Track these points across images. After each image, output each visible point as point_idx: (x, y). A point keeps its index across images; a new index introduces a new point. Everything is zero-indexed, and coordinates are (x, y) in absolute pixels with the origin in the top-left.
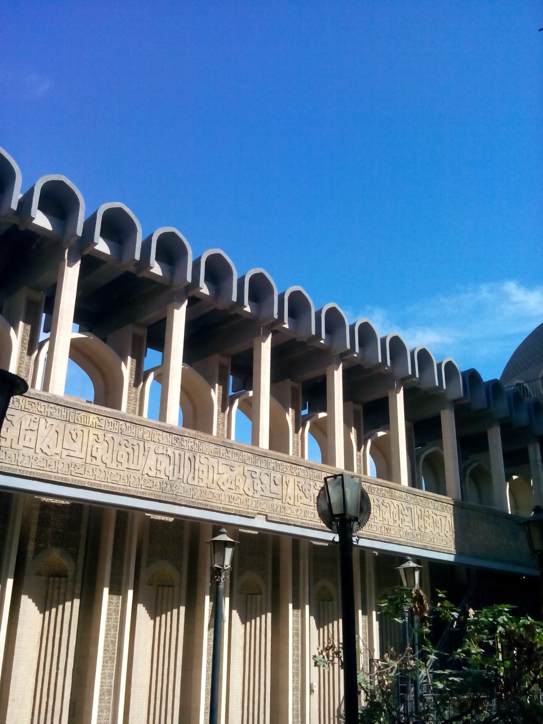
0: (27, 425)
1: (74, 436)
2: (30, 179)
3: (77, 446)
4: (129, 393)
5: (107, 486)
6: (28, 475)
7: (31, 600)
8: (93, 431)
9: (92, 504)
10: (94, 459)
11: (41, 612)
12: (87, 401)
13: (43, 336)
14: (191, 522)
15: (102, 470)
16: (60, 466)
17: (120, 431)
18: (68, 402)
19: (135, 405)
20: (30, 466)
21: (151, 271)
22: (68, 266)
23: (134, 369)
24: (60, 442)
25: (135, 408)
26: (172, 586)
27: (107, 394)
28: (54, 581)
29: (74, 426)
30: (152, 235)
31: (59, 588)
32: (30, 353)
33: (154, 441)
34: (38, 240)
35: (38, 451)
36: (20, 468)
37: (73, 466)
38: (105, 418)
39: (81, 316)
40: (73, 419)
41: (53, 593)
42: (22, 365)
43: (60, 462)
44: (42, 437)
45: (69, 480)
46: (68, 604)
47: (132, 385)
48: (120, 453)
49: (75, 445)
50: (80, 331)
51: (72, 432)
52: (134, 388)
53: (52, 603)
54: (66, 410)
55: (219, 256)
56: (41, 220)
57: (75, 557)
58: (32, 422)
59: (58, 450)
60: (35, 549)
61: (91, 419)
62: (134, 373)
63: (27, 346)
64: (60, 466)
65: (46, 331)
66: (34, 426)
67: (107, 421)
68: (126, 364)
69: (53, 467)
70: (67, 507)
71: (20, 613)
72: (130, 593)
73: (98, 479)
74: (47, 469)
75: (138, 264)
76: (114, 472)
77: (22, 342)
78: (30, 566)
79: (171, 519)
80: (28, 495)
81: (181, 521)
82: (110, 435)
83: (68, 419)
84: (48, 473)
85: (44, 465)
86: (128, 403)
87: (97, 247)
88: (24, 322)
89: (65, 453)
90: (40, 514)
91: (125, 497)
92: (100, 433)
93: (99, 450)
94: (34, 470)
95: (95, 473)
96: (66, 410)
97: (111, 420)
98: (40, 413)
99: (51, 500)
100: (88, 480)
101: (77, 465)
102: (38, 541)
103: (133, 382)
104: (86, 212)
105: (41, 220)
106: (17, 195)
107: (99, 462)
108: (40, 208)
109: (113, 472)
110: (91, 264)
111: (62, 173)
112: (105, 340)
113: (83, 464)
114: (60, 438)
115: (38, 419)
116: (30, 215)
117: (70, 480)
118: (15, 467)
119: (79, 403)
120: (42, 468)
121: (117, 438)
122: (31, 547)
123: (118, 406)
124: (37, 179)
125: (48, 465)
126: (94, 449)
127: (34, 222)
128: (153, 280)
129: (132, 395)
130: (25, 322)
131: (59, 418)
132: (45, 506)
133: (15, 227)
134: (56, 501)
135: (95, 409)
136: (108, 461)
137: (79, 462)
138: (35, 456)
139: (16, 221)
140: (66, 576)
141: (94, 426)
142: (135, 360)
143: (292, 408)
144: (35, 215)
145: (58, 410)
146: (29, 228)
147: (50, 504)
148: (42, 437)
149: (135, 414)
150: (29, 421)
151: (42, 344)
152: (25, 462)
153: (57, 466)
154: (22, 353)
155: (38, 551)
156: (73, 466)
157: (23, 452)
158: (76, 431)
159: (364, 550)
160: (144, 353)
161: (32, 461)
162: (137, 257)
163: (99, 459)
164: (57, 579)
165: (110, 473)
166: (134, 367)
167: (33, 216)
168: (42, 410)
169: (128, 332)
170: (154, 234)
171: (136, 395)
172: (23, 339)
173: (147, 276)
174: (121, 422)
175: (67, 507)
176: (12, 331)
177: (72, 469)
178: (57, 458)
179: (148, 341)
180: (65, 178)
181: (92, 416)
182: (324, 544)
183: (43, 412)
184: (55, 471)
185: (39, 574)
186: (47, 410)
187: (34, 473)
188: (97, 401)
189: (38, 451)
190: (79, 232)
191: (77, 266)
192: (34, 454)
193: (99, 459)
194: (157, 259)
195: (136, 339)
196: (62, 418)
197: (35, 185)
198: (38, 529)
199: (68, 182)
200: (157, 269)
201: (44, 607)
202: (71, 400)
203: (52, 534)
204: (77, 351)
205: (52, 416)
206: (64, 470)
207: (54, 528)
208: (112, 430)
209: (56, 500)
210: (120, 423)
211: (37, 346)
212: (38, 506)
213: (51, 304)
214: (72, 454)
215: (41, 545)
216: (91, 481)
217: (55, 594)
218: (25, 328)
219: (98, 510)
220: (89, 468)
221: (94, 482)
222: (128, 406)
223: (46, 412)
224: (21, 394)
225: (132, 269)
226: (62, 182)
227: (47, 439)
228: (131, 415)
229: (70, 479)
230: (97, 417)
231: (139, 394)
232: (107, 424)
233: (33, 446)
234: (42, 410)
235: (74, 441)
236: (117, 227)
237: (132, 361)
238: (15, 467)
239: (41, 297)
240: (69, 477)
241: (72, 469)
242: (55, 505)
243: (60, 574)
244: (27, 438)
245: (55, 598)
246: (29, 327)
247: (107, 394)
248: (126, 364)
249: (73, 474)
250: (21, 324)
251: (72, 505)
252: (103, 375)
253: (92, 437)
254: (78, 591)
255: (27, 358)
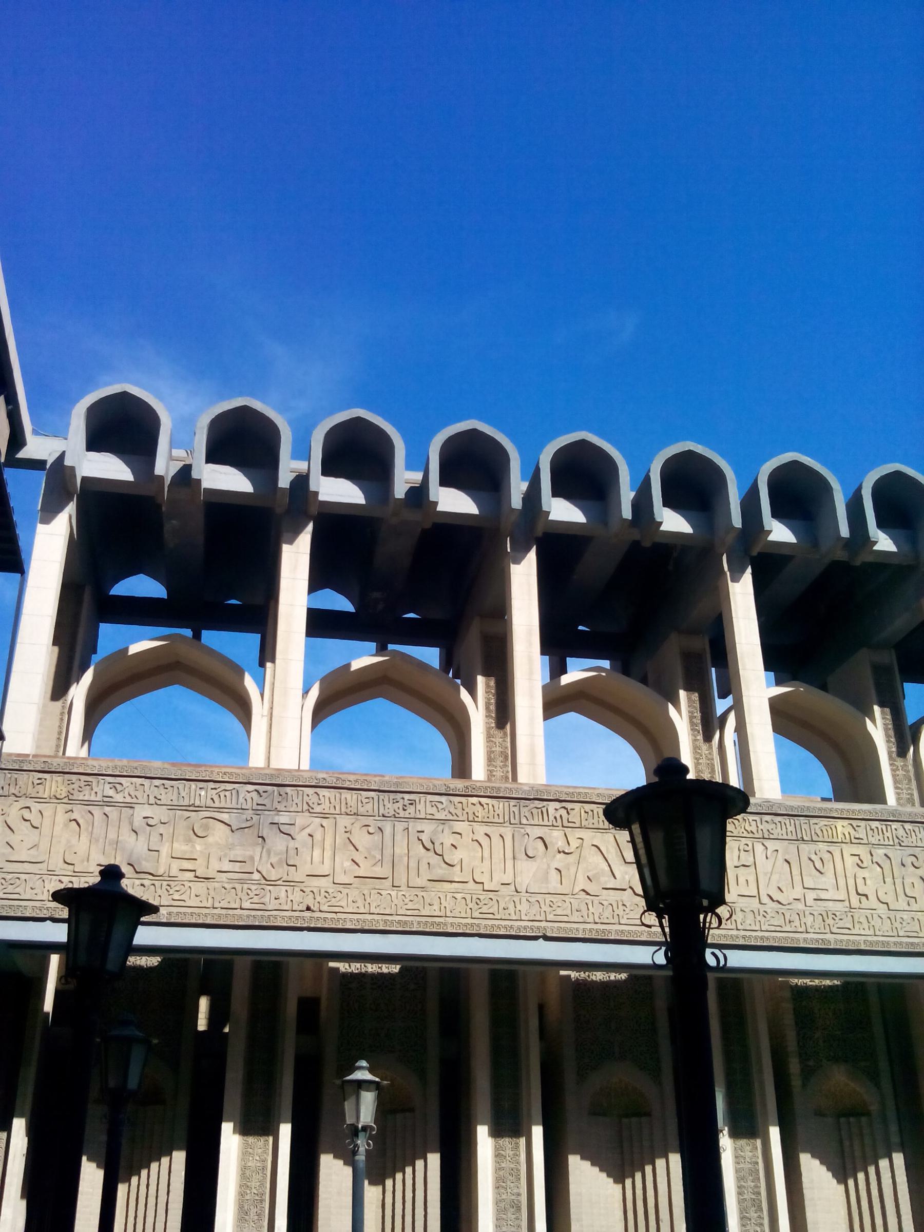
0: (736, 858)
1: (818, 865)
2: (639, 463)
3: (827, 880)
4: (892, 770)
5: (901, 943)
6: (759, 944)
7: (817, 1162)
8: (848, 850)
9: (882, 980)
10: (863, 898)
11: (839, 1182)
12: (823, 799)
13: (721, 705)
14: (442, 969)
15: (882, 916)
16: (809, 920)
17: (896, 841)
18: (792, 808)
19: (909, 788)
20: (543, 918)
21: (875, 548)
22: (732, 581)
23: (890, 726)
24: (797, 878)
25: (912, 795)
26: (412, 1110)
27: (854, 780)
28: (849, 1123)
29: (812, 847)
30: (859, 489)
31: (861, 1135)
32: (708, 738)
33: (383, 816)
34: (675, 555)
35: (765, 899)
36: (742, 933)
37: (830, 916)
38: (862, 823)
39: (777, 660)
40: (517, 817)
41: (852, 1146)
42: (700, 761)
43: (807, 913)
44: (766, 874)
45: (829, 942)
46: (660, 1163)
47: (894, 755)
48: (908, 881)
49: (823, 879)
50: (779, 683)
51: (813, 857)
52: (899, 759)
53: (854, 1163)
54: (792, 821)
55: (689, 456)
56: (673, 522)
57: (873, 1076)
58: (742, 852)
59: (798, 892)
60: (802, 1070)
61: (840, 829)
62: (892, 733)
63: (700, 728)
64: (809, 920)
65: (723, 696)
66: (747, 859)
67: (868, 828)
68: (873, 720)
69: (797, 923)
70: (838, 991)
71: (804, 1186)
72: (774, 1133)
73: (881, 933)
74: (788, 928)
75: (848, 544)
76: (905, 916)
77: (692, 724)
78: (800, 1103)
79: (395, 969)
80: (766, 977)
81: (416, 969)
82: (881, 852)
83: (799, 836)
84: (791, 935)
85: (781, 922)
86: (896, 788)
87: (772, 538)
88: (484, 675)
89: (811, 896)
90: (794, 1009)
91: (31, 923)
92: (862, 851)
93: (868, 882)
94: (766, 934)
95: (873, 923)
96: (792, 821)
97: (874, 824)
98: (751, 835)
99: (808, 982)
100: (864, 938)
101: (837, 914)
102: (804, 1056)
103: (894, 749)
104: (739, 488)
105: (454, 502)
106: (627, 495)
107: (873, 902)
108: (667, 503)
109: (905, 917)
110: (768, 567)
111: (685, 439)
112: (824, 687)
113: (847, 910)
114: (796, 872)
115: (750, 845)
116: (869, 538)
117: (832, 942)
118: (735, 932)
119: (812, 805)
120: (778, 929)
121: (896, 854)
122: (794, 1066)
123: (880, 798)
124: (651, 461)
125: (787, 921)
126: (860, 881)
127: (440, 508)
128: (883, 562)
129: (900, 772)
130: (486, 674)
131: (785, 837)
132: (800, 993)
133: (636, 544)
134: (817, 982)
135: (842, 810)
136: (890, 899)
137: (839, 907)
138: (762, 908)
139: (635, 535)
140: (868, 1114)
141: (848, 840)
142: (887, 710)
143: (882, 705)
144: (550, 506)
145: (779, 824)
146: (658, 540)
147: (807, 988)
148: (766, 874)
149: (913, 805)
150: (736, 852)
151: (723, 719)
152: (748, 922)
153: (803, 920)
154: (695, 740)
155: (808, 1073)
156: (830, 916)
157: (741, 905)
158: (819, 855)
159: (736, 983)
160: (901, 694)
161: (759, 918)
162: (844, 531)
163: (872, 897)
164: (852, 1119)
165: (899, 920)
166: (889, 722)
167: (659, 520)
168: (754, 829)
169: (862, 665)
170: (864, 485)
171: (908, 771)
172: (691, 718)
173: (870, 559)
174: (895, 825)
175: (838, 991)
176: (464, 695)
177: (831, 922)
178: (800, 906)
179: (902, 671)
180: (693, 443)
181: (840, 823)
182: (385, 969)
183: (755, 832)
184: (803, 929)
185: (819, 1113)
186: (761, 827)
187: (767, 939)
188: (840, 795)
189: (765, 899)
190: (737, 521)
191: (747, 577)
192: (804, 908)
193: (872, 897)
194: (880, 525)
195: (880, 671)
196: (790, 837)
197: (649, 471)
198: (798, 1034)
199: (699, 449)
200: (884, 543)
201: (842, 1173)
202: (796, 802)
203: (824, 1042)
204: (784, 717)
205: (772, 836)
206: (817, 926)
207: (824, 1029)
208: (882, 842)
209: (817, 981)
210: (893, 827)
211: (716, 723)
212: (787, 994)
213: (720, 649)
214: (823, 895)
215: (811, 1063)
216: (869, 938)
217: (857, 1147)
218: (689, 699)
219: (453, 971)
220: (860, 916)
221: (875, 938)
222: (898, 794)
223: (760, 832)
224: (744, 810)
225: (841, 555)
226: (690, 452)
227: (775, 877)
228: (909, 809)
229: (833, 941)
230: (847, 823)
231: (911, 768)
232: (870, 833)
233: (755, 893)
234: (754, 829)
235: (821, 873)
236: (797, 494)
237: (883, 713)
238: (735, 932)
239: (702, 644)
240: (829, 936)
241: (831, 922)
242: (817, 989)
243: (851, 1111)
244: (742, 880)
245: (858, 1153)
246: (695, 696)
247: (854, 780)
248: (873, 720)
249: (835, 930)
250: (682, 694)
251: (846, 985)
252: (836, 746)
253: (850, 861)
254: (895, 1139)
255: (704, 747)
